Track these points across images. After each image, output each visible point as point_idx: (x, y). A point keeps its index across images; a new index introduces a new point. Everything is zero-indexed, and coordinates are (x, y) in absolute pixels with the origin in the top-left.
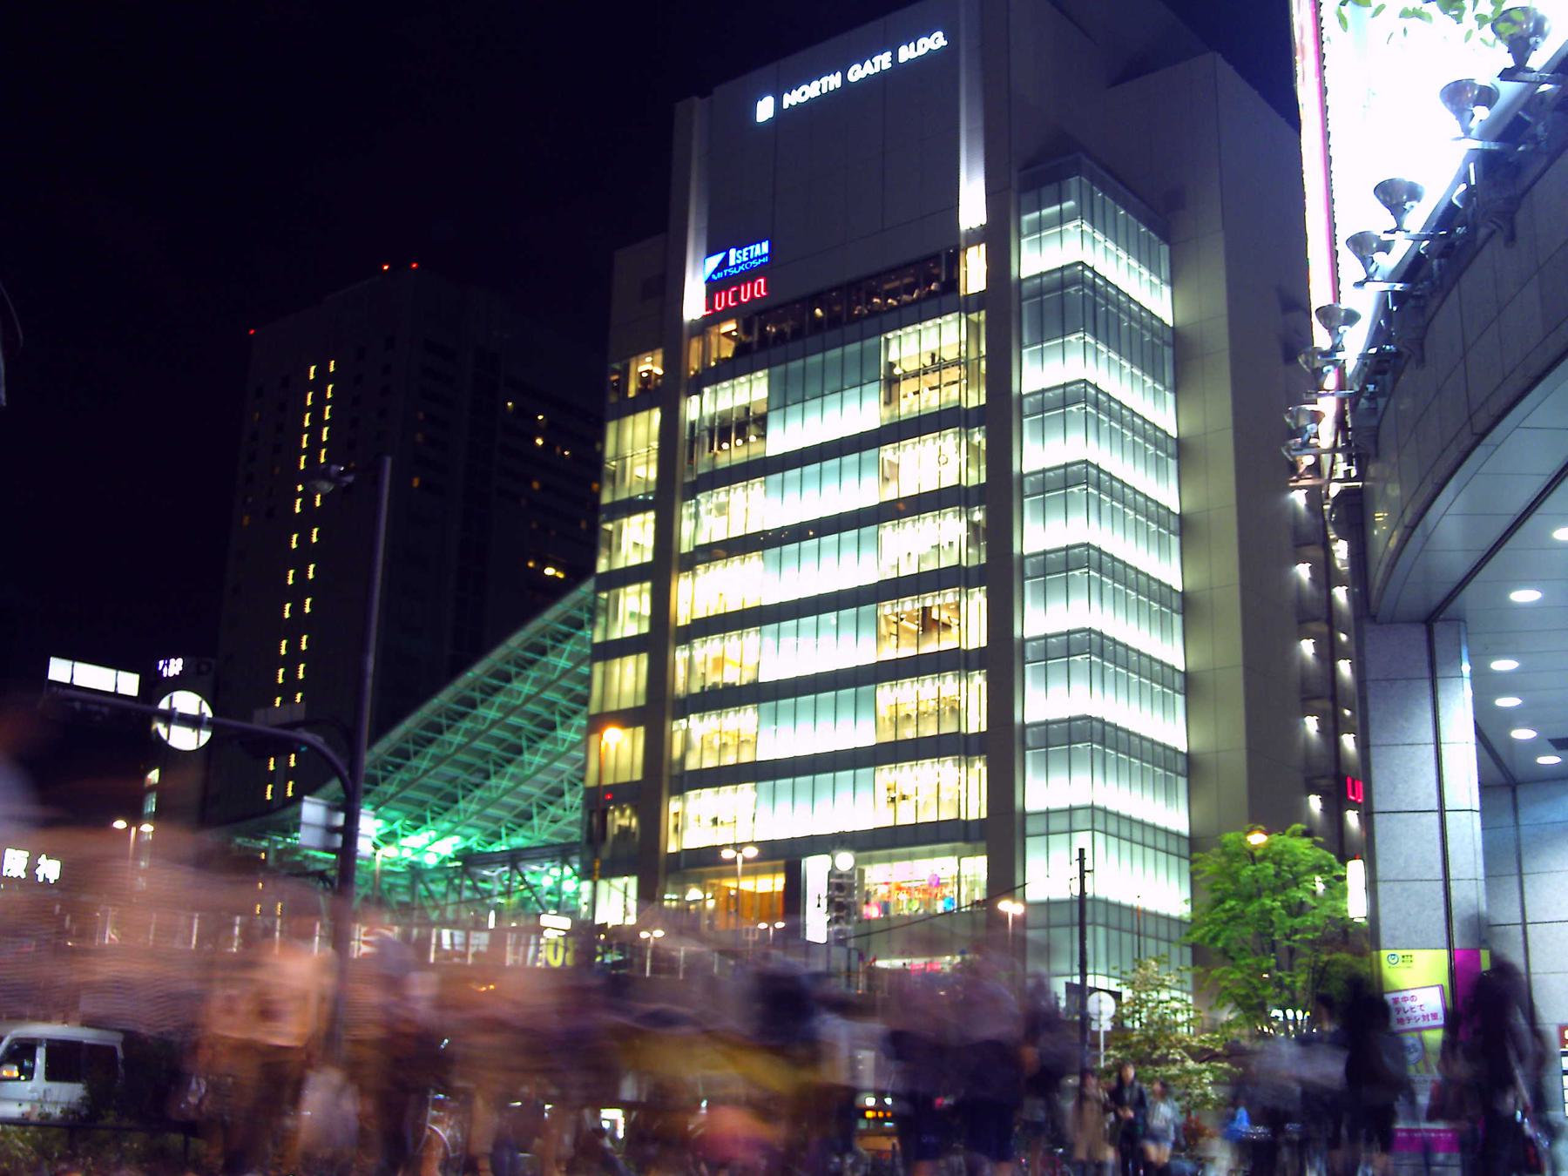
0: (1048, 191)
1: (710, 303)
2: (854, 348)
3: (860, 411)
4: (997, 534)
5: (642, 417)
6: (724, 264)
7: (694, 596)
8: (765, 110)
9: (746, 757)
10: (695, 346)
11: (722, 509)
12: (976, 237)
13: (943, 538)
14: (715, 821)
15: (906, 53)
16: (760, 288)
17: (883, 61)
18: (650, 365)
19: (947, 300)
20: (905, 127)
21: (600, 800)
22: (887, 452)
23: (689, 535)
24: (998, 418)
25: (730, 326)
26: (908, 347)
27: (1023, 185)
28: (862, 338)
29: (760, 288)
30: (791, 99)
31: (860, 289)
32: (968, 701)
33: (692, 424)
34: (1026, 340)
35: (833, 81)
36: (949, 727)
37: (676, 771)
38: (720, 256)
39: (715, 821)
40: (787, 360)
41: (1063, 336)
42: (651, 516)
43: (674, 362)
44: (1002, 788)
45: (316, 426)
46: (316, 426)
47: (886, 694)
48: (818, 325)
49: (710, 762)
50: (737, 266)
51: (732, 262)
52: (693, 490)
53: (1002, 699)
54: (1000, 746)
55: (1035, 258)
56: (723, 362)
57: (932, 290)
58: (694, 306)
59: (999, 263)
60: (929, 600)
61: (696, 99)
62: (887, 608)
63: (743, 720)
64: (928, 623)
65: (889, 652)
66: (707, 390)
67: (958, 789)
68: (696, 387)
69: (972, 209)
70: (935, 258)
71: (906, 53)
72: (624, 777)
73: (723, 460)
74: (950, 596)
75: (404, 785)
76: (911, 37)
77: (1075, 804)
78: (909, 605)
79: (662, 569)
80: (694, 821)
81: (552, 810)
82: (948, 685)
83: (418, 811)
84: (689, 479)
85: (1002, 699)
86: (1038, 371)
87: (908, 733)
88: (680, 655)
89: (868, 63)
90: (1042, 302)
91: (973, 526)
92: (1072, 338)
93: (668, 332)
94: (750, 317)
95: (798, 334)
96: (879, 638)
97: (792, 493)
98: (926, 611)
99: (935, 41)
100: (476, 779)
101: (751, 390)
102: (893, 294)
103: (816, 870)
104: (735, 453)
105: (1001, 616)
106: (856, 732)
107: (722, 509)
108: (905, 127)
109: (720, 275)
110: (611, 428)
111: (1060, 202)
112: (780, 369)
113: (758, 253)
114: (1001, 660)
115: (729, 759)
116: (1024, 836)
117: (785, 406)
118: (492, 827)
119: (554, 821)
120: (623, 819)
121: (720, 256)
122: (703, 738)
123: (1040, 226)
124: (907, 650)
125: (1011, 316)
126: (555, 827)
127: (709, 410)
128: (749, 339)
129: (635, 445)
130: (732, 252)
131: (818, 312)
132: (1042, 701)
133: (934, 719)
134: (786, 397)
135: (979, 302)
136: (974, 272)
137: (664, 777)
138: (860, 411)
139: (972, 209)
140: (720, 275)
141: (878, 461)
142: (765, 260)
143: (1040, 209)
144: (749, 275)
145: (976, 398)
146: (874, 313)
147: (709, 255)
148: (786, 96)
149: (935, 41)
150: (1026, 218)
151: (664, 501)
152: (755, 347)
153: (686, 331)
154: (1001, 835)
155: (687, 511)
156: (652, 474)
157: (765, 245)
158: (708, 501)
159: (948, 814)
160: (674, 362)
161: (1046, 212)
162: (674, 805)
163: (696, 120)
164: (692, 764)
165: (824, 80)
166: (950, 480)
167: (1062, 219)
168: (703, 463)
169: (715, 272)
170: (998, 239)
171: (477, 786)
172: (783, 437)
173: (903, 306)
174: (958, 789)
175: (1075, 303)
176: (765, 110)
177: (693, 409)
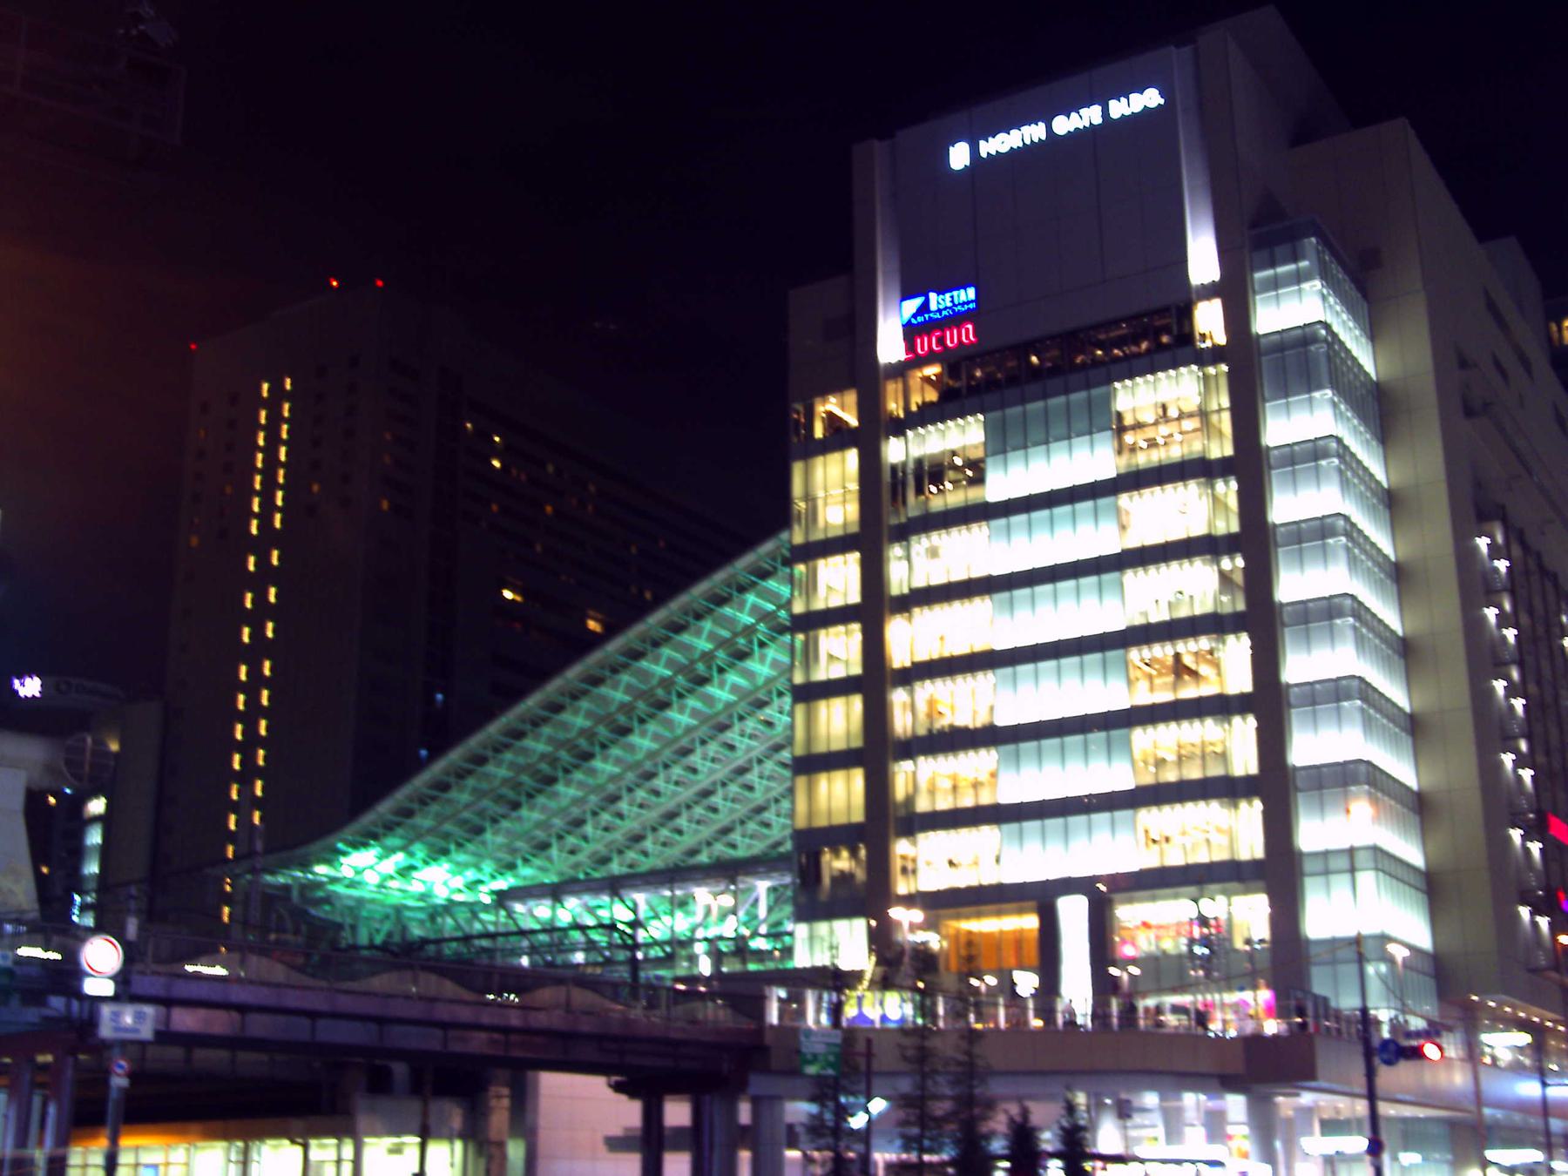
0: (1280, 251)
1: (910, 348)
2: (1078, 397)
3: (1092, 460)
4: (1259, 581)
5: (834, 458)
6: (924, 308)
7: (908, 639)
8: (959, 156)
9: (986, 799)
10: (892, 390)
11: (933, 553)
12: (1209, 292)
13: (1198, 586)
14: (951, 863)
15: (1118, 109)
16: (968, 333)
17: (1091, 115)
18: (842, 407)
19: (1182, 352)
20: (1123, 187)
21: (813, 842)
22: (1124, 499)
23: (901, 574)
24: (1249, 467)
25: (932, 371)
26: (1136, 397)
27: (1254, 243)
28: (1088, 386)
29: (968, 333)
30: (989, 147)
31: (1075, 340)
32: (1239, 743)
33: (894, 468)
34: (1267, 394)
35: (1035, 132)
36: (1215, 771)
37: (902, 812)
38: (919, 301)
39: (951, 863)
40: (1002, 406)
41: (1309, 391)
42: (854, 558)
43: (870, 405)
44: (1279, 827)
45: (272, 444)
46: (272, 444)
47: (1144, 739)
48: (1036, 374)
49: (944, 803)
50: (940, 311)
51: (933, 307)
52: (903, 533)
53: (1272, 742)
54: (1275, 787)
55: (1276, 314)
56: (925, 407)
57: (1167, 341)
58: (890, 346)
59: (1238, 317)
60: (1180, 646)
61: (876, 144)
62: (1134, 654)
63: (980, 762)
64: (1180, 669)
65: (1144, 696)
66: (910, 433)
67: (1240, 831)
68: (898, 427)
69: (1203, 259)
70: (1163, 311)
71: (1118, 109)
72: (840, 819)
73: (937, 504)
74: (1204, 643)
75: (441, 818)
76: (1123, 92)
77: (1357, 844)
78: (1163, 651)
79: (873, 609)
80: (932, 862)
81: (571, 840)
82: (1205, 731)
83: (443, 844)
84: (894, 521)
85: (1272, 742)
86: (1284, 426)
87: (1170, 776)
88: (898, 697)
89: (1073, 115)
90: (1283, 359)
91: (1224, 578)
92: (1317, 394)
93: (864, 376)
94: (955, 362)
95: (1013, 380)
96: (1130, 682)
97: (1019, 537)
98: (1177, 656)
99: (1151, 98)
100: (500, 810)
101: (963, 435)
102: (1120, 342)
103: (1073, 913)
104: (952, 497)
105: (1266, 662)
106: (1115, 776)
107: (933, 553)
108: (1123, 187)
109: (920, 319)
110: (797, 469)
111: (1295, 260)
112: (997, 414)
113: (963, 298)
114: (1269, 703)
115: (967, 801)
116: (1302, 875)
117: (1004, 452)
118: (508, 858)
119: (572, 852)
120: (840, 862)
121: (919, 301)
122: (925, 781)
123: (1275, 284)
124: (1164, 696)
125: (1255, 371)
126: (573, 859)
127: (917, 451)
128: (957, 385)
129: (830, 489)
130: (933, 296)
131: (1034, 359)
132: (1310, 745)
133: (1198, 762)
134: (1002, 442)
135: (1216, 355)
136: (1209, 320)
137: (887, 820)
138: (1092, 460)
139: (1203, 259)
140: (920, 319)
141: (1118, 511)
142: (972, 306)
143: (1273, 265)
144: (956, 318)
145: (1221, 448)
146: (1096, 363)
147: (904, 298)
148: (982, 143)
149: (1151, 98)
150: (1258, 275)
151: (870, 541)
152: (964, 391)
153: (882, 374)
154: (1280, 873)
155: (896, 551)
156: (853, 510)
157: (971, 293)
158: (920, 544)
159: (1220, 855)
160: (870, 405)
161: (1281, 270)
162: (901, 847)
163: (876, 163)
164: (923, 805)
165: (1025, 129)
166: (1198, 530)
167: (1299, 278)
168: (913, 506)
169: (915, 316)
170: (1235, 294)
171: (504, 817)
172: (1002, 483)
173: (1127, 357)
174: (1240, 831)
175: (1303, 361)
176: (959, 156)
177: (895, 451)
